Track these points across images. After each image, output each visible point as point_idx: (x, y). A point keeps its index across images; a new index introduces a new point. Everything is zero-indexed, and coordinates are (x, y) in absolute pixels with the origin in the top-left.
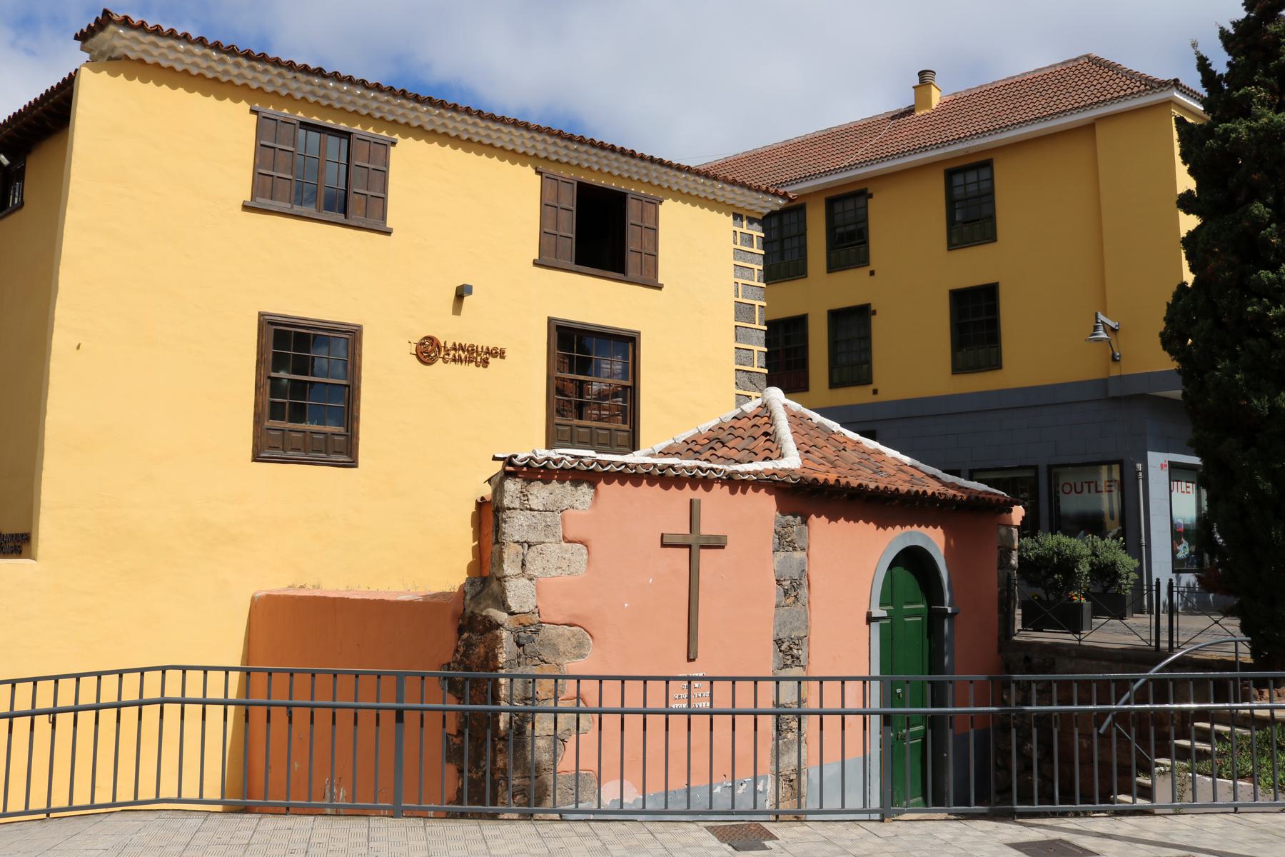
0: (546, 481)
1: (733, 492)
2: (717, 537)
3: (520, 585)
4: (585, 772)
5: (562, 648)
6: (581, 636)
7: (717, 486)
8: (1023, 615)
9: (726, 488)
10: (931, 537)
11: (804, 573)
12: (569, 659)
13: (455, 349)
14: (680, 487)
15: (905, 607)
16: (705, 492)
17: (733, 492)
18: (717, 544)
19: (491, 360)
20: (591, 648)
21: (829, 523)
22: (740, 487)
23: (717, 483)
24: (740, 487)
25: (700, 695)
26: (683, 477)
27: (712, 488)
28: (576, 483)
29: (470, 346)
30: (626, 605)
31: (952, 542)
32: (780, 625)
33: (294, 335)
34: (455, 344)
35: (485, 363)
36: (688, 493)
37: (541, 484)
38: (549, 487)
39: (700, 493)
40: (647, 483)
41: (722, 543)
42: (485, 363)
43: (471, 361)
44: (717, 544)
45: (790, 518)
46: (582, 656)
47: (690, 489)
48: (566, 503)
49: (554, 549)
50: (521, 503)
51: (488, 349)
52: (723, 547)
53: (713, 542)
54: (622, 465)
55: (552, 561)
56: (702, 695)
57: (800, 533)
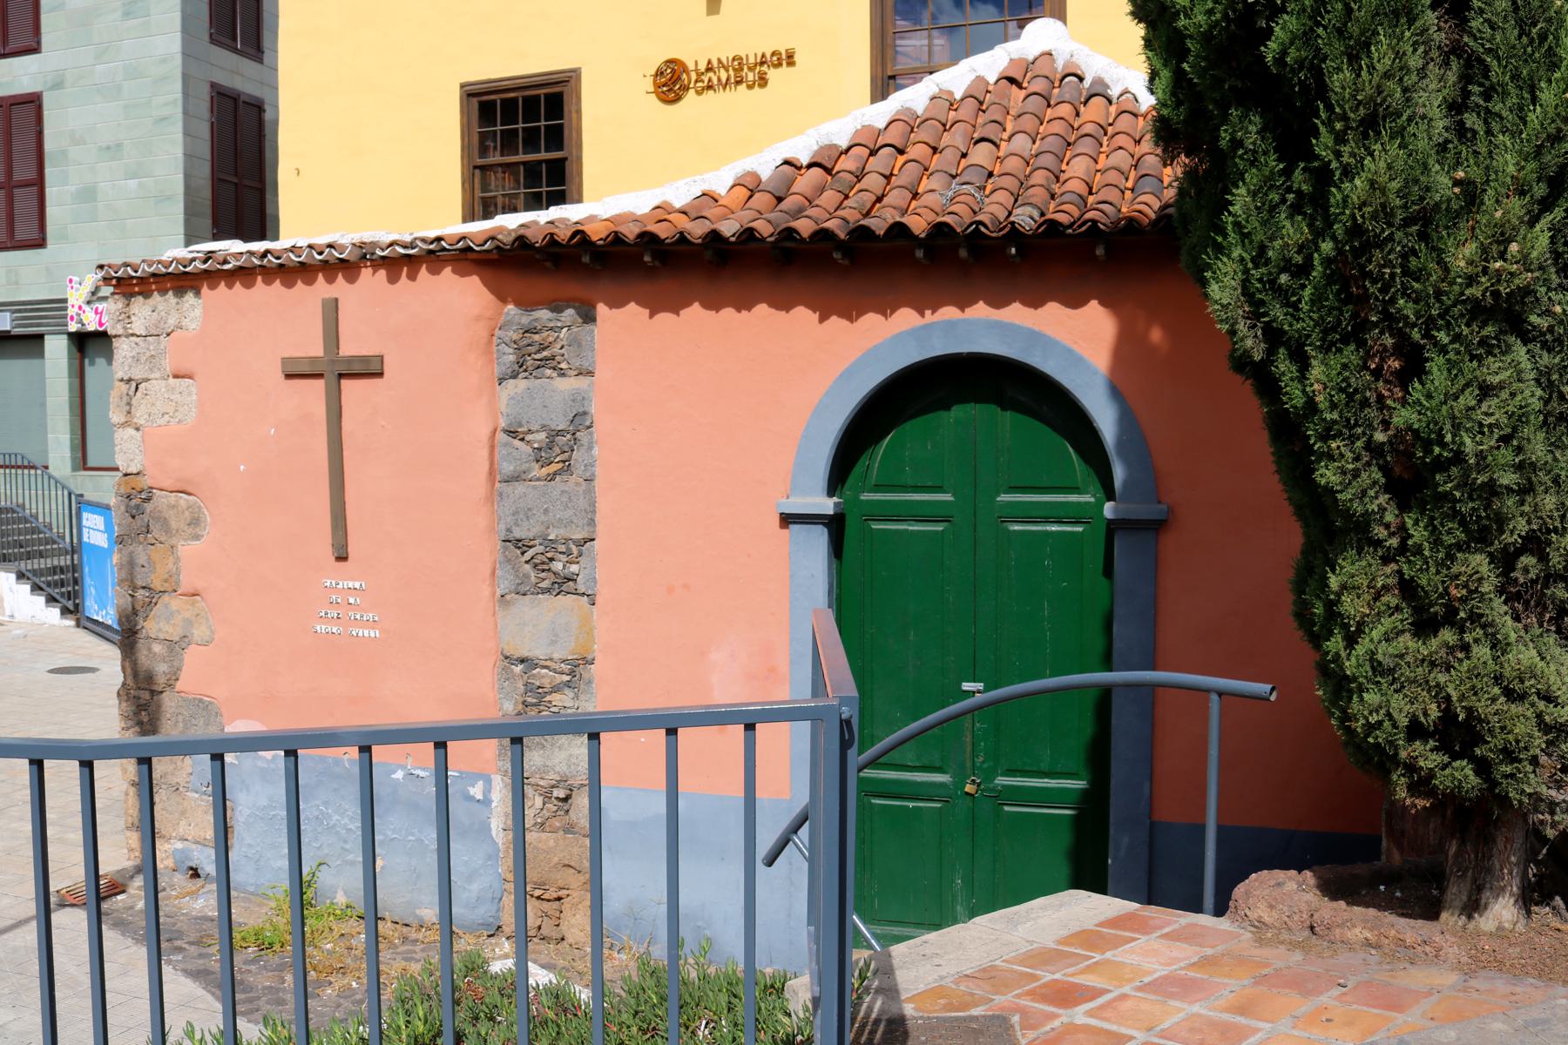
0: (147, 294)
1: (393, 279)
2: (364, 359)
3: (125, 437)
4: (208, 699)
5: (174, 524)
6: (197, 510)
7: (366, 273)
8: (1078, 532)
9: (382, 273)
10: (1049, 331)
11: (580, 420)
12: (185, 540)
13: (709, 69)
14: (310, 282)
15: (1004, 498)
16: (348, 285)
17: (393, 279)
18: (370, 370)
19: (772, 74)
20: (208, 528)
21: (651, 316)
22: (405, 269)
23: (366, 267)
24: (405, 269)
25: (358, 617)
26: (310, 265)
27: (359, 275)
28: (180, 291)
29: (773, 54)
30: (242, 467)
31: (1156, 335)
32: (515, 513)
33: (545, 99)
34: (709, 62)
35: (763, 81)
36: (322, 288)
37: (140, 298)
38: (150, 301)
39: (340, 285)
40: (264, 281)
41: (374, 368)
42: (763, 81)
43: (738, 83)
44: (370, 370)
45: (544, 314)
46: (197, 537)
47: (344, 281)
48: (172, 321)
49: (157, 387)
50: (125, 328)
51: (719, 61)
52: (380, 375)
53: (357, 368)
54: (172, 262)
55: (158, 403)
56: (362, 616)
57: (575, 342)
